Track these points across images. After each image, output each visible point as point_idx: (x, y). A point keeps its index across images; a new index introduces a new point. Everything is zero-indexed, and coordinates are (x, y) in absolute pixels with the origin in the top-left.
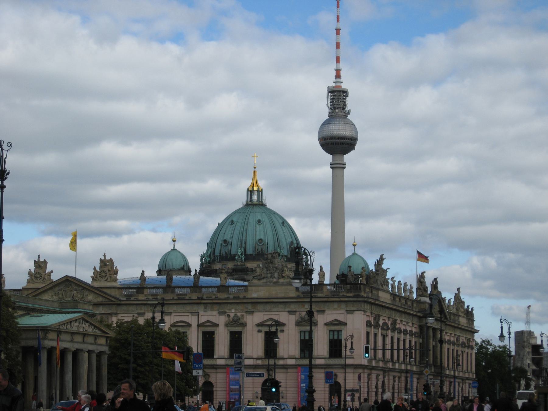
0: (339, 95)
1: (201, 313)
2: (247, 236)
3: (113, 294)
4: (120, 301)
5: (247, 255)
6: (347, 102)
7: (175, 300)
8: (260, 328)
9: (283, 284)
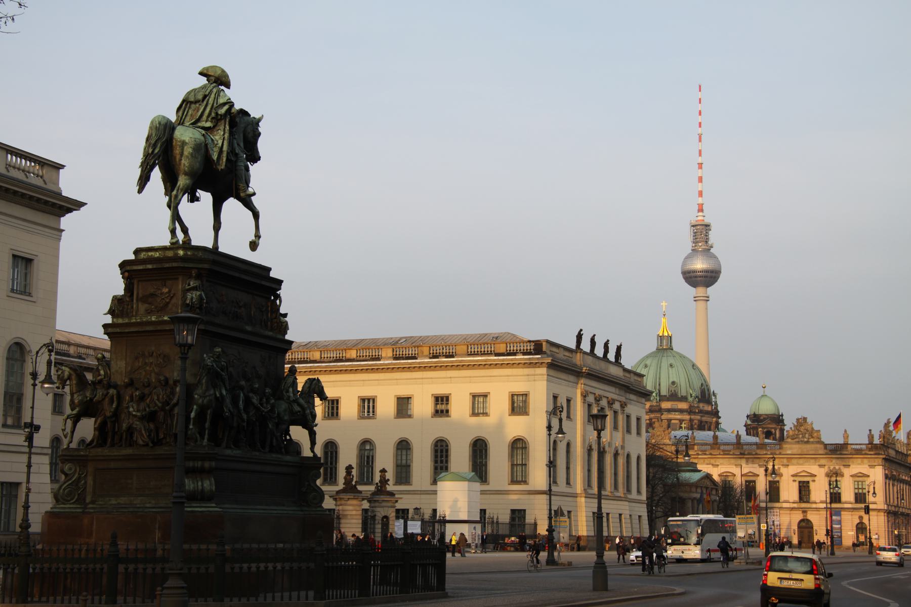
1: (744, 465)
3: (669, 450)
5: (662, 396)
7: (722, 455)
9: (813, 443)
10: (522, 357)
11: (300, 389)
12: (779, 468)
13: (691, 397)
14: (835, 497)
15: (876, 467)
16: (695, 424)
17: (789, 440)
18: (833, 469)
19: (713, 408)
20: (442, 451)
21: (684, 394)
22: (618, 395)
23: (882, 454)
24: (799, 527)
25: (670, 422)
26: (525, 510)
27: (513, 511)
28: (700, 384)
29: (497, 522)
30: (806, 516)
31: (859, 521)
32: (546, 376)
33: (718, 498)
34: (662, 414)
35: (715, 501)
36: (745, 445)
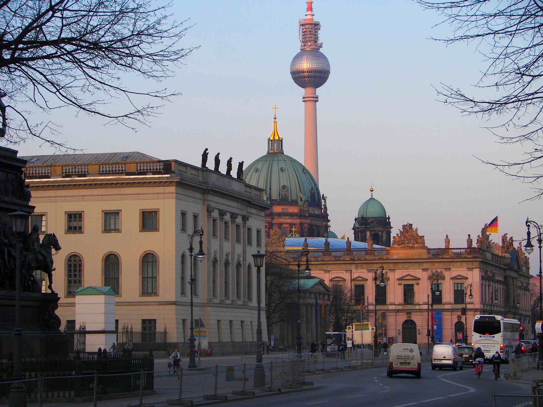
0: (311, 28)
1: (354, 270)
2: (272, 182)
4: (290, 262)
6: (319, 35)
8: (400, 282)
10: (152, 176)
11: (41, 242)
12: (386, 273)
13: (301, 200)
14: (437, 299)
15: (474, 269)
16: (305, 228)
17: (396, 246)
18: (435, 272)
19: (323, 212)
20: (75, 266)
21: (294, 198)
22: (240, 209)
23: (479, 258)
24: (403, 328)
25: (281, 226)
26: (155, 320)
27: (144, 321)
28: (310, 188)
29: (131, 332)
30: (410, 317)
31: (457, 321)
32: (175, 195)
33: (330, 303)
34: (273, 218)
35: (327, 305)
36: (354, 251)
